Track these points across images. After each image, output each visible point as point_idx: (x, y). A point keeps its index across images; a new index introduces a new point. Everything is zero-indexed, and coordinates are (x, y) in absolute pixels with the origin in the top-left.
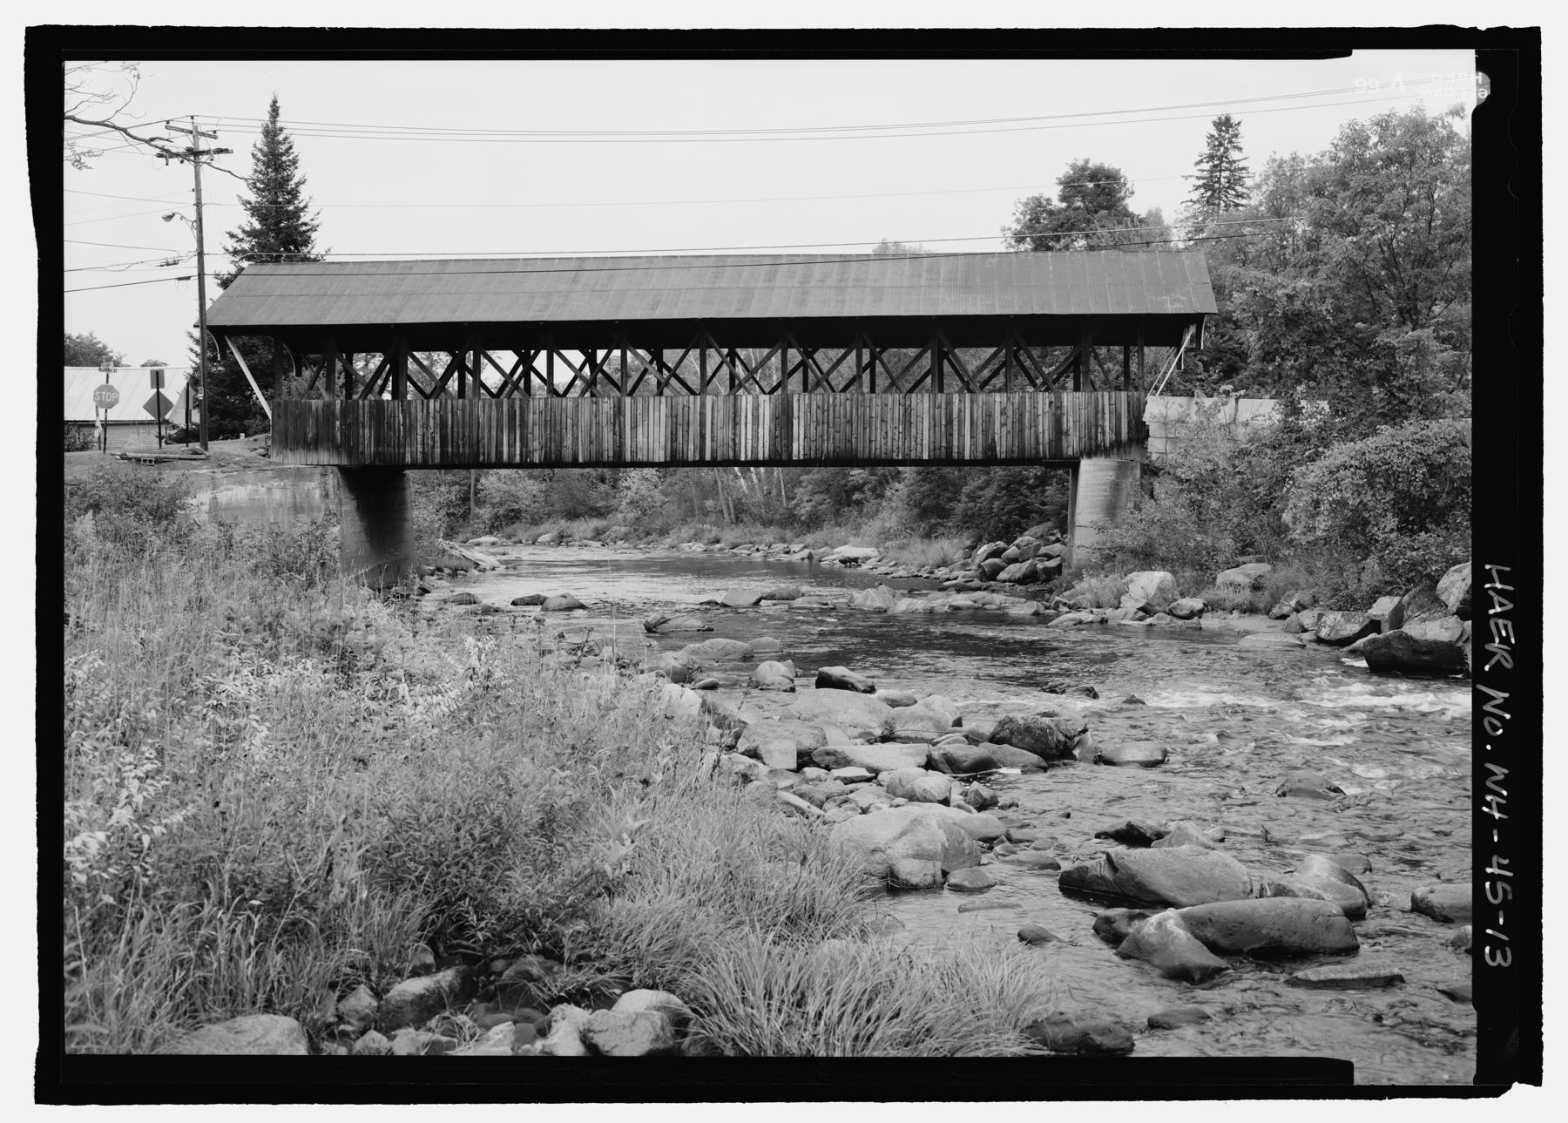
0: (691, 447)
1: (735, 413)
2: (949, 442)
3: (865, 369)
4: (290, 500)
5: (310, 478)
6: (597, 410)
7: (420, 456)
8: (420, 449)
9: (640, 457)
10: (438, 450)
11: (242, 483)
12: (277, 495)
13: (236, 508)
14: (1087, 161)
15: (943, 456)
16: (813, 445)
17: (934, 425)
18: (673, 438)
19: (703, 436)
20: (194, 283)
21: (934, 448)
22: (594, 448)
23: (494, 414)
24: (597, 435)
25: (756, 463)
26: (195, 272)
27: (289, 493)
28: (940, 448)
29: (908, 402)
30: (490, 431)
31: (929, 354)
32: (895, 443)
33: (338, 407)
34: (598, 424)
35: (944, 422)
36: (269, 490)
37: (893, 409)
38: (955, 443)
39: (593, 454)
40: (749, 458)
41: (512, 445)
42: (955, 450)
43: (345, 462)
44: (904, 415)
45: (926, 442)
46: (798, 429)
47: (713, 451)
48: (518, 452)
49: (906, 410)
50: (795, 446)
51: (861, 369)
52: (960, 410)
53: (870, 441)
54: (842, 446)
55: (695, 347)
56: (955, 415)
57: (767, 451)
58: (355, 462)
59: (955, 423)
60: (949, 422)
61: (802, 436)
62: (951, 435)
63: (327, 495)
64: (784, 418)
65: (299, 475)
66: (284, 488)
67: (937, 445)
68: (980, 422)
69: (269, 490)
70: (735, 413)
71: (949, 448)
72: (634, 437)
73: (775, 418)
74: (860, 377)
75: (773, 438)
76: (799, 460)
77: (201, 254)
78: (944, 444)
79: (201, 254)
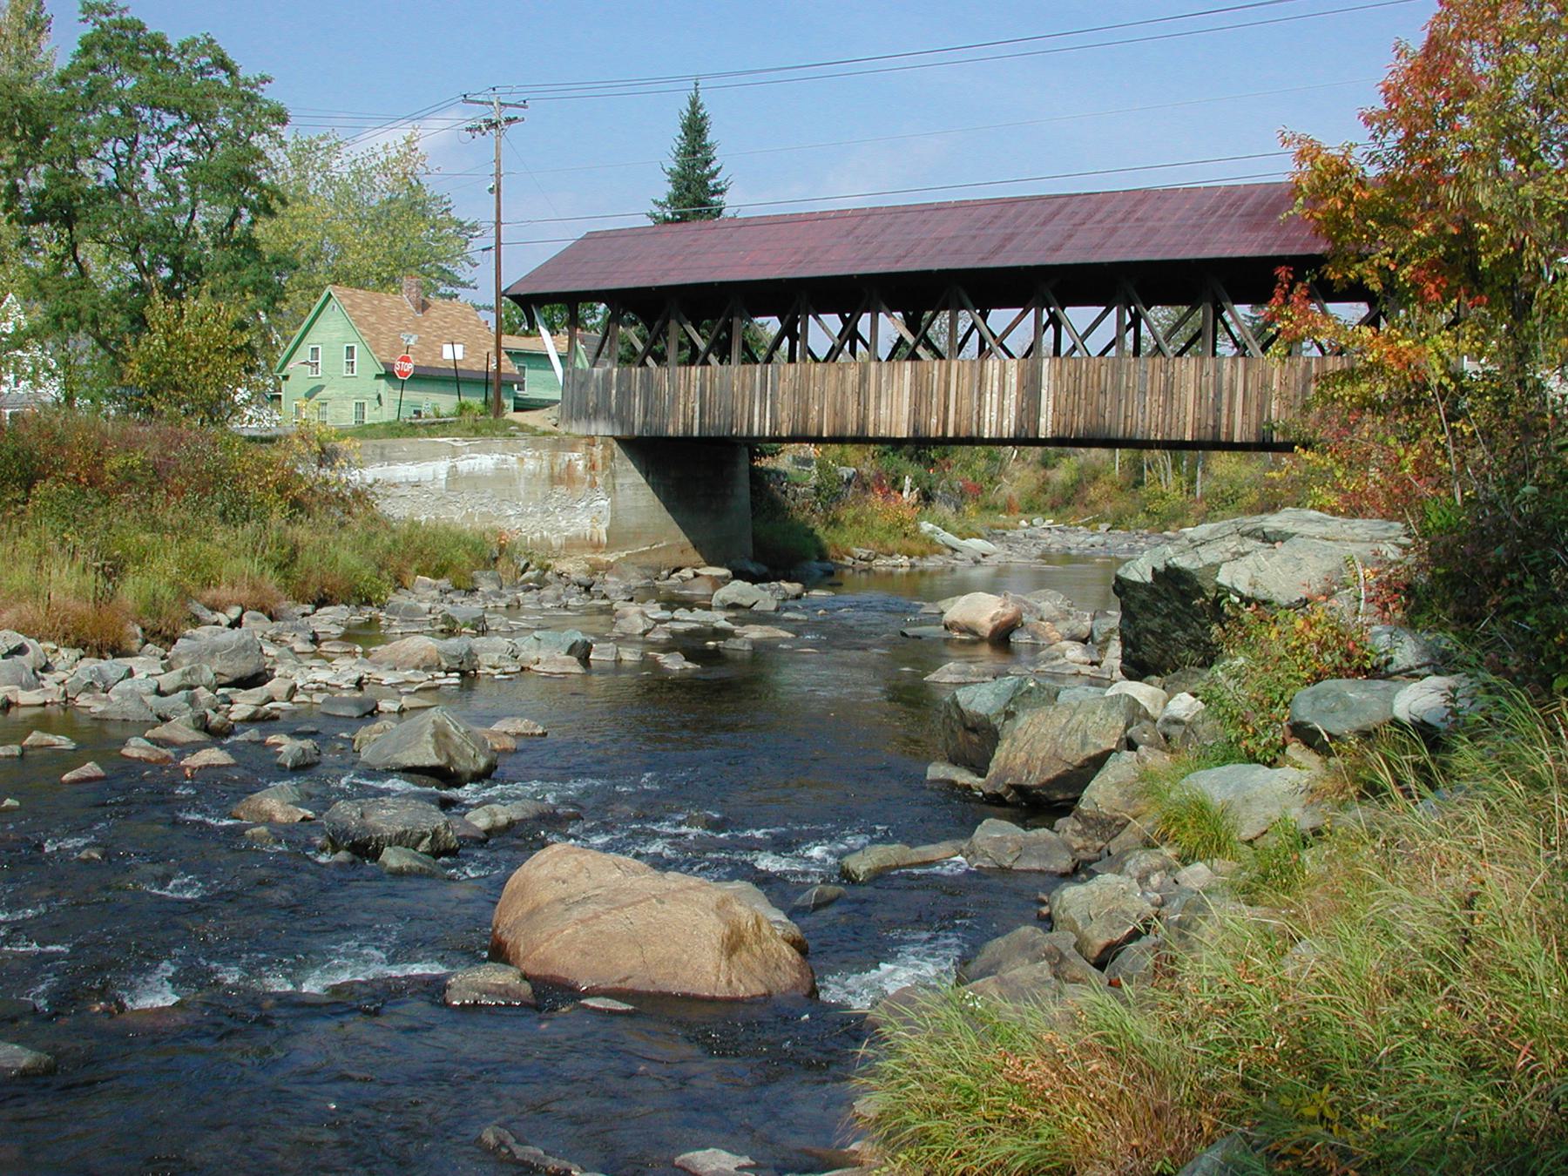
0: (934, 420)
1: (981, 381)
2: (1217, 420)
3: (1128, 328)
4: (546, 472)
5: (572, 448)
6: (844, 377)
7: (681, 428)
8: (681, 420)
9: (882, 431)
10: (697, 422)
11: (487, 452)
12: (531, 465)
13: (479, 477)
14: (1401, 52)
15: (1209, 438)
16: (1062, 420)
17: (1199, 398)
18: (916, 411)
19: (946, 408)
20: (493, 252)
21: (1197, 428)
22: (838, 422)
23: (748, 380)
24: (842, 403)
25: (1001, 442)
26: (493, 243)
27: (545, 464)
28: (1206, 428)
29: (1170, 369)
30: (743, 401)
31: (1200, 313)
32: (1154, 419)
33: (615, 374)
34: (844, 393)
35: (1211, 395)
36: (521, 460)
37: (1152, 378)
38: (1224, 421)
39: (838, 427)
40: (993, 435)
41: (762, 416)
42: (1224, 430)
43: (618, 433)
44: (1166, 385)
45: (1189, 419)
46: (1046, 403)
47: (957, 426)
48: (768, 424)
49: (1167, 379)
50: (1042, 420)
51: (1039, 330)
52: (1231, 379)
53: (1126, 417)
54: (1094, 422)
55: (946, 309)
56: (1225, 386)
57: (1012, 430)
58: (626, 433)
59: (1225, 395)
60: (1218, 394)
61: (1050, 408)
62: (1219, 410)
63: (593, 467)
64: (1030, 387)
65: (562, 444)
66: (540, 457)
67: (1203, 421)
68: (1255, 394)
69: (521, 460)
70: (981, 381)
71: (1216, 427)
72: (878, 407)
73: (1022, 386)
74: (1123, 337)
75: (1020, 410)
76: (1046, 439)
77: (498, 223)
78: (1211, 422)
79: (498, 223)
